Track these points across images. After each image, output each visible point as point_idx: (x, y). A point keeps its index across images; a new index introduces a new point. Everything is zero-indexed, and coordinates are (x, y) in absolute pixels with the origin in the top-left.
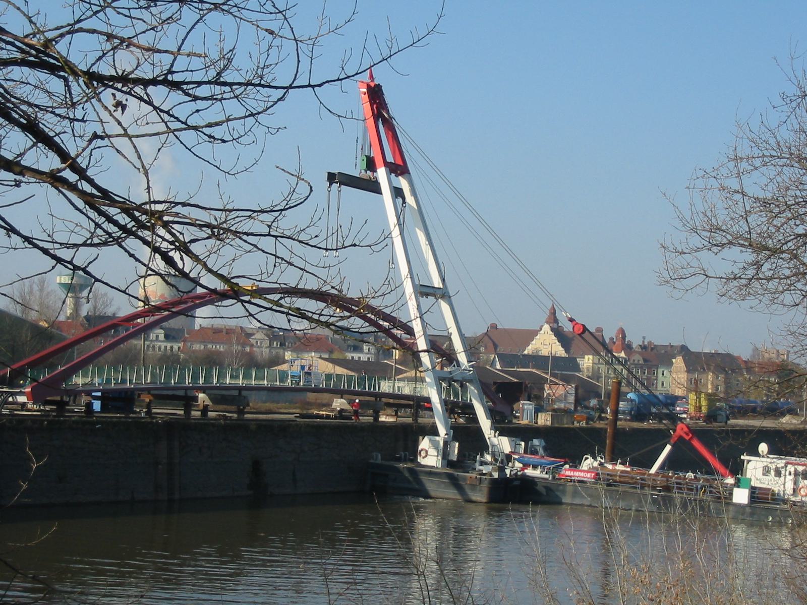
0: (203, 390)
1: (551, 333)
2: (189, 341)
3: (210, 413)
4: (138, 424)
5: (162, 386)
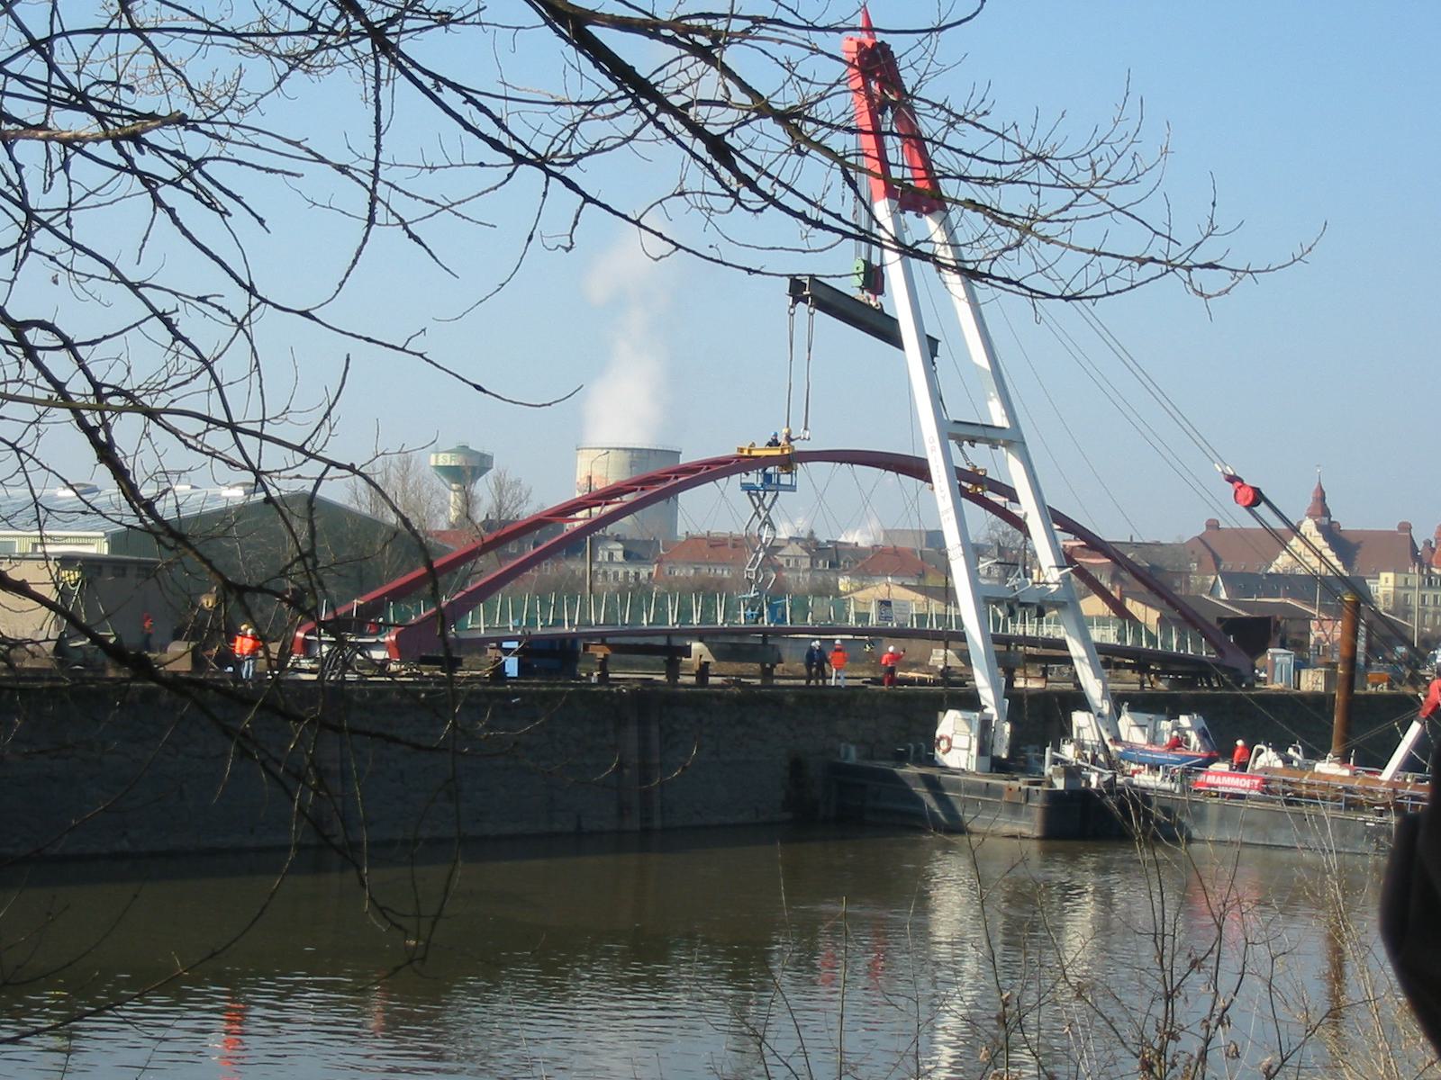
0: (700, 635)
1: (1317, 534)
2: (668, 562)
3: (711, 679)
4: (586, 695)
5: (627, 628)
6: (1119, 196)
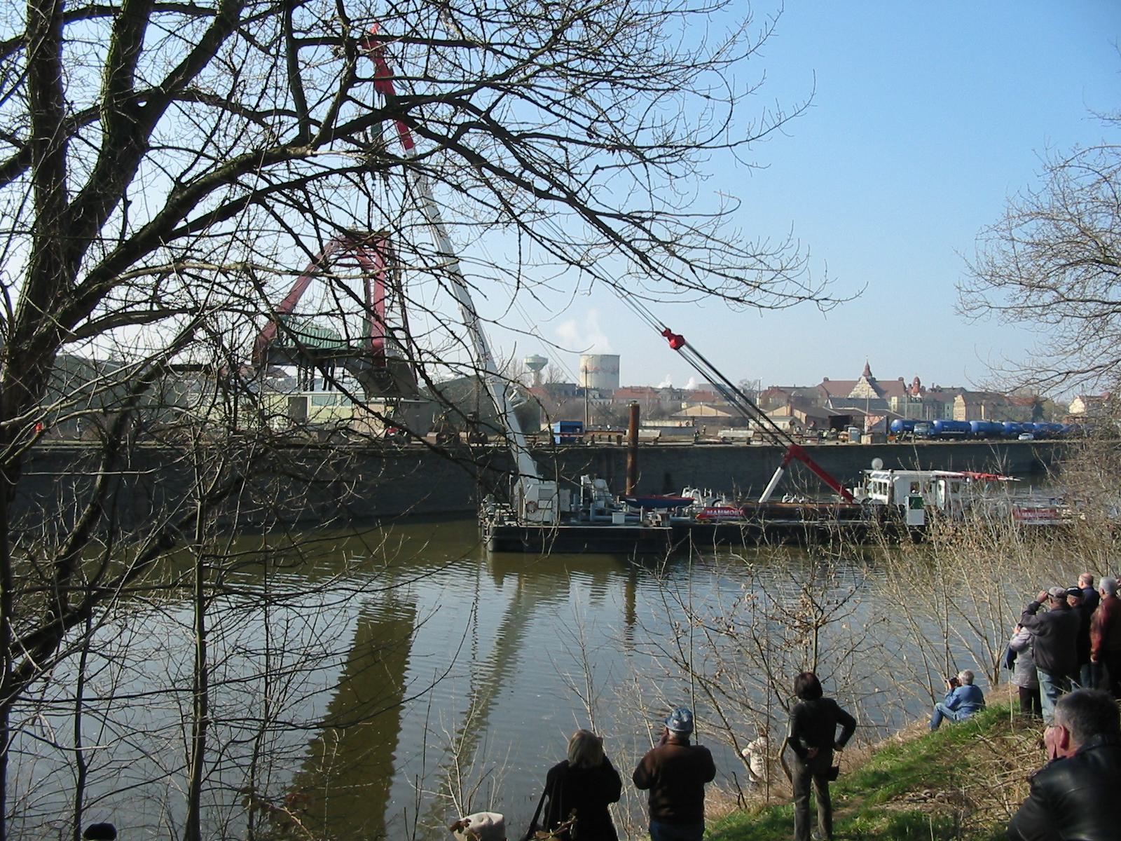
6: (790, 274)
